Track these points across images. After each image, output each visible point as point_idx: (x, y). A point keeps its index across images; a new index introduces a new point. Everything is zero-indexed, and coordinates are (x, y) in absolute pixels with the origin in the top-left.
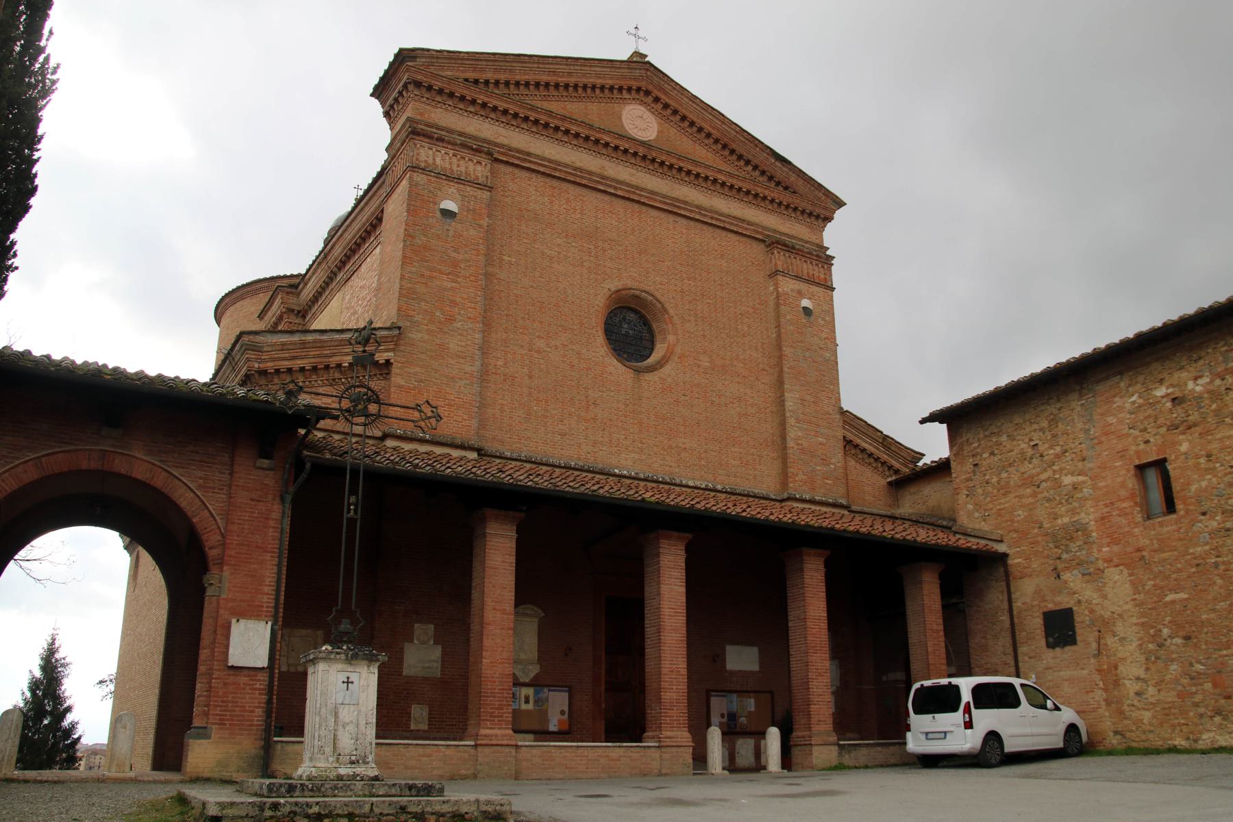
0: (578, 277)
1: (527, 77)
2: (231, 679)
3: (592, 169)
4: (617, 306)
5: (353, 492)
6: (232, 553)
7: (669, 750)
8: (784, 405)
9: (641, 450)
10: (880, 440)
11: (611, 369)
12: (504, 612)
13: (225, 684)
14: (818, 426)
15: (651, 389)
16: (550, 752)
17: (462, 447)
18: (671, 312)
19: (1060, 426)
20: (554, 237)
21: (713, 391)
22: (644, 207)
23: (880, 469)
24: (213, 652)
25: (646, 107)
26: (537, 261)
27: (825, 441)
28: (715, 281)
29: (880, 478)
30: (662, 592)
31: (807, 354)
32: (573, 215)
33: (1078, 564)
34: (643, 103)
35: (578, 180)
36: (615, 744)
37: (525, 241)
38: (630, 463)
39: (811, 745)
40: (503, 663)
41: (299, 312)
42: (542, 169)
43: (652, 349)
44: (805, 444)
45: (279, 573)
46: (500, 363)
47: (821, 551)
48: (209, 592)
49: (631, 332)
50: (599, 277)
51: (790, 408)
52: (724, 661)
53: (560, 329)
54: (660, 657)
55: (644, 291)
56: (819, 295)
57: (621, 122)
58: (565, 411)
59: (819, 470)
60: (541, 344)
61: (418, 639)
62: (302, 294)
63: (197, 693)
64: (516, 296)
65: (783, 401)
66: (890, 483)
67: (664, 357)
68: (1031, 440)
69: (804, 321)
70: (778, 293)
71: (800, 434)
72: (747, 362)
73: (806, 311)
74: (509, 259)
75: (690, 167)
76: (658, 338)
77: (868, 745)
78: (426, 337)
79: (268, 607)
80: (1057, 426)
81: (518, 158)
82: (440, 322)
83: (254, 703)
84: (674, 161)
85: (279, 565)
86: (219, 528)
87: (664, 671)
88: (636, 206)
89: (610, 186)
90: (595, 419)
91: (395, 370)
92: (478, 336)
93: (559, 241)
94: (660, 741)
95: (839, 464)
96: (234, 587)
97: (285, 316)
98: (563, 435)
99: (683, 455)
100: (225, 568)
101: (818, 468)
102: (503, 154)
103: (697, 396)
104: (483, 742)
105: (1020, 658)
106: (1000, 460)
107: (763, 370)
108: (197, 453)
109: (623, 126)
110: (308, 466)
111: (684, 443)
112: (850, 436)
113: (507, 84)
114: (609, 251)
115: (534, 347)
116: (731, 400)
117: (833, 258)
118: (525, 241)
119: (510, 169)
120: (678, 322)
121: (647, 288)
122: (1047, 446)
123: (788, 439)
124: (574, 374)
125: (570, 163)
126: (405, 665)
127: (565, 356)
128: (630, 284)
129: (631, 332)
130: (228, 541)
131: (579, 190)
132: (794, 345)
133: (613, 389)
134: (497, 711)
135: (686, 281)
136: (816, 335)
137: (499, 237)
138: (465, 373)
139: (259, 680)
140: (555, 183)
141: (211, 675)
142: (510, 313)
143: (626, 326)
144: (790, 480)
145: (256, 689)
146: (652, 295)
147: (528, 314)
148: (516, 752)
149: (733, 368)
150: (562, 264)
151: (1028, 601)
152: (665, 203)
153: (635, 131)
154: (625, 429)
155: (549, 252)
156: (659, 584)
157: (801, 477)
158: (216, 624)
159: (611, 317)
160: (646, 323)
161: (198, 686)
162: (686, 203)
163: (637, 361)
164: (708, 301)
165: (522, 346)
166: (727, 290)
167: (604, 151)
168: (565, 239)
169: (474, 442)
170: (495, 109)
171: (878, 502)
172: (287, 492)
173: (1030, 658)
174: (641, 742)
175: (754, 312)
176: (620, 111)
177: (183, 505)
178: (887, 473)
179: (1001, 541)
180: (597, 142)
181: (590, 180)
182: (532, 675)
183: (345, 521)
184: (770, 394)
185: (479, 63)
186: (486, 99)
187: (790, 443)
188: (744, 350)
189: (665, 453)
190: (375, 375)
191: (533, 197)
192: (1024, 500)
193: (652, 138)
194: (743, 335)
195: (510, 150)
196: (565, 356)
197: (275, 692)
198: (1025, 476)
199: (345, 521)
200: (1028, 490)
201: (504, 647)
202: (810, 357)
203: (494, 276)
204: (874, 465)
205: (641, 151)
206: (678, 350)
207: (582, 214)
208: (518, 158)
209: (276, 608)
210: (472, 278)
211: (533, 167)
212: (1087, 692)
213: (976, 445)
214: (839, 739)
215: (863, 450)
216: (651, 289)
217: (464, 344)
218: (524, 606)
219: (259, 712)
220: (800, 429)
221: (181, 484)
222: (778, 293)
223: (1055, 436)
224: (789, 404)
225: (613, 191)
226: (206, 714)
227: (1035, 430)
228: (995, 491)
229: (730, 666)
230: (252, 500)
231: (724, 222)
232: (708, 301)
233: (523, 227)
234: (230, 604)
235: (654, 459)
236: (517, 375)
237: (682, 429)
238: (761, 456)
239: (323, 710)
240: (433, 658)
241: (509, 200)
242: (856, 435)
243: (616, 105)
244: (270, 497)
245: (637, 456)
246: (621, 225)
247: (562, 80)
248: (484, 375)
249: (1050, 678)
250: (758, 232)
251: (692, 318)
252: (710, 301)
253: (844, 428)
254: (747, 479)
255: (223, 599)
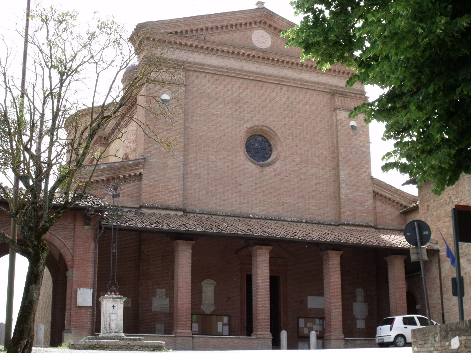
0: (231, 123)
1: (201, 26)
2: (78, 311)
3: (237, 67)
4: (252, 135)
5: (114, 242)
6: (77, 263)
7: (261, 339)
8: (339, 178)
9: (264, 205)
10: (395, 192)
11: (248, 166)
12: (186, 282)
13: (76, 313)
14: (358, 186)
15: (269, 175)
16: (207, 340)
17: (176, 210)
18: (279, 135)
19: (460, 188)
20: (218, 104)
21: (302, 173)
22: (264, 83)
23: (396, 206)
24: (71, 301)
25: (265, 30)
26: (210, 118)
27: (362, 194)
28: (303, 117)
29: (396, 211)
30: (258, 272)
31: (353, 150)
32: (227, 93)
33: (465, 255)
34: (263, 28)
35: (229, 75)
36: (236, 337)
37: (204, 108)
38: (258, 211)
39: (330, 339)
40: (187, 303)
41: (105, 138)
42: (211, 72)
43: (271, 154)
44: (351, 196)
45: (95, 270)
46: (193, 169)
47: (338, 252)
48: (68, 279)
49: (259, 147)
50: (241, 122)
51: (342, 179)
52: (306, 303)
53: (222, 150)
54: (257, 300)
55: (265, 126)
56: (361, 118)
57: (252, 40)
58: (225, 189)
59: (359, 209)
60: (213, 158)
61: (158, 295)
62: (106, 129)
63: (66, 316)
64: (200, 136)
65: (339, 175)
66: (401, 213)
67: (275, 159)
68: (449, 194)
69: (351, 133)
70: (337, 120)
71: (348, 192)
72: (320, 157)
73: (353, 127)
74: (196, 118)
75: (288, 60)
76: (273, 148)
77: (361, 340)
78: (158, 160)
79: (91, 283)
80: (459, 188)
81: (199, 68)
82: (163, 153)
83: (87, 320)
84: (279, 58)
85: (95, 267)
86: (71, 254)
87: (258, 306)
88: (260, 83)
89: (246, 75)
90: (240, 192)
91: (144, 177)
92: (182, 158)
93: (221, 106)
94: (257, 336)
95: (370, 206)
96: (78, 276)
97: (99, 140)
98: (224, 200)
99: (286, 206)
100: (74, 269)
101: (358, 208)
102: (191, 67)
103: (293, 176)
104: (178, 335)
105: (444, 301)
106: (437, 204)
107: (329, 160)
108: (61, 225)
109: (252, 43)
110: (103, 228)
111: (286, 200)
112: (377, 190)
113: (192, 31)
114: (247, 108)
115: (381, 10)
116: (311, 177)
117: (368, 98)
118: (204, 108)
119: (196, 73)
120: (283, 140)
121: (266, 125)
122: (454, 197)
123: (341, 195)
124: (229, 171)
125: (225, 66)
126: (153, 307)
127: (225, 163)
128: (257, 123)
129: (259, 147)
130: (75, 259)
131: (230, 79)
132: (346, 146)
133: (249, 176)
134: (184, 323)
135: (287, 119)
136: (358, 140)
137: (191, 108)
138: (176, 176)
139: (89, 311)
140: (218, 77)
141: (71, 309)
142: (198, 144)
143: (257, 144)
144: (342, 215)
145: (88, 315)
146: (269, 128)
147: (206, 144)
148: (193, 339)
149: (313, 160)
150: (222, 118)
151: (447, 273)
152: (275, 80)
153: (259, 44)
154: (256, 196)
155: (215, 112)
156: (257, 269)
157: (348, 213)
158: (72, 290)
159: (249, 140)
160: (267, 141)
161: (66, 314)
162: (286, 78)
163: (263, 161)
164: (299, 127)
165: (204, 160)
166: (309, 121)
167: (242, 58)
168: (224, 105)
169: (181, 206)
170: (186, 45)
171: (394, 223)
172: (96, 238)
173: (447, 300)
174: (251, 336)
175: (325, 131)
176: (251, 35)
177: (57, 245)
178: (400, 208)
179: (437, 244)
180: (238, 53)
181: (235, 73)
182: (211, 311)
183: (112, 253)
184: (333, 172)
185: (177, 23)
186: (181, 41)
187: (343, 197)
188: (319, 151)
189: (276, 205)
190: (135, 180)
191: (207, 86)
192: (446, 224)
193: (268, 46)
194: (318, 143)
195: (195, 65)
196: (225, 163)
197: (95, 316)
198: (447, 212)
199: (112, 253)
200: (447, 219)
201: (187, 297)
202: (355, 151)
203: (189, 127)
204: (392, 204)
205: (262, 55)
206: (283, 154)
207: (232, 91)
208: (199, 68)
209: (94, 283)
210: (178, 131)
211: (206, 71)
212: (468, 316)
213: (428, 196)
214: (345, 337)
215: (385, 197)
216: (268, 125)
217: (175, 162)
218: (207, 280)
219: (89, 323)
220: (348, 189)
221: (56, 237)
222: (337, 120)
223: (457, 192)
224: (342, 177)
225: (247, 78)
226: (70, 324)
227: (450, 190)
228: (435, 219)
229: (309, 306)
230: (83, 242)
231: (308, 85)
232: (299, 127)
233: (203, 102)
234: (77, 283)
235: (270, 209)
236: (201, 174)
237: (285, 193)
238: (327, 204)
239: (106, 315)
240: (165, 303)
241: (195, 89)
242: (380, 190)
243: (249, 32)
244: (90, 240)
245: (262, 208)
246: (252, 94)
247: (219, 25)
248: (185, 176)
249: (454, 310)
250: (326, 88)
251: (290, 137)
252: (300, 128)
253: (373, 186)
254: (320, 216)
255: (74, 281)
